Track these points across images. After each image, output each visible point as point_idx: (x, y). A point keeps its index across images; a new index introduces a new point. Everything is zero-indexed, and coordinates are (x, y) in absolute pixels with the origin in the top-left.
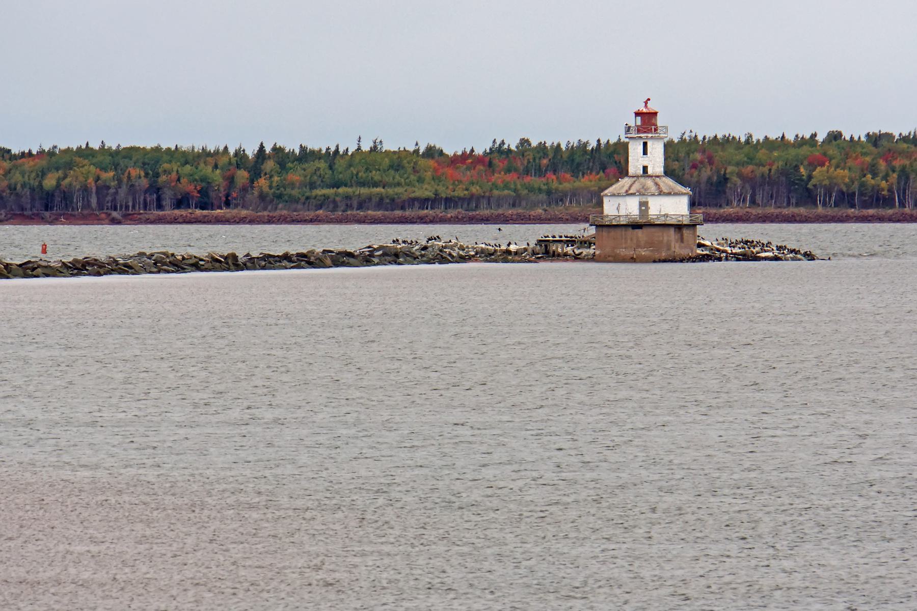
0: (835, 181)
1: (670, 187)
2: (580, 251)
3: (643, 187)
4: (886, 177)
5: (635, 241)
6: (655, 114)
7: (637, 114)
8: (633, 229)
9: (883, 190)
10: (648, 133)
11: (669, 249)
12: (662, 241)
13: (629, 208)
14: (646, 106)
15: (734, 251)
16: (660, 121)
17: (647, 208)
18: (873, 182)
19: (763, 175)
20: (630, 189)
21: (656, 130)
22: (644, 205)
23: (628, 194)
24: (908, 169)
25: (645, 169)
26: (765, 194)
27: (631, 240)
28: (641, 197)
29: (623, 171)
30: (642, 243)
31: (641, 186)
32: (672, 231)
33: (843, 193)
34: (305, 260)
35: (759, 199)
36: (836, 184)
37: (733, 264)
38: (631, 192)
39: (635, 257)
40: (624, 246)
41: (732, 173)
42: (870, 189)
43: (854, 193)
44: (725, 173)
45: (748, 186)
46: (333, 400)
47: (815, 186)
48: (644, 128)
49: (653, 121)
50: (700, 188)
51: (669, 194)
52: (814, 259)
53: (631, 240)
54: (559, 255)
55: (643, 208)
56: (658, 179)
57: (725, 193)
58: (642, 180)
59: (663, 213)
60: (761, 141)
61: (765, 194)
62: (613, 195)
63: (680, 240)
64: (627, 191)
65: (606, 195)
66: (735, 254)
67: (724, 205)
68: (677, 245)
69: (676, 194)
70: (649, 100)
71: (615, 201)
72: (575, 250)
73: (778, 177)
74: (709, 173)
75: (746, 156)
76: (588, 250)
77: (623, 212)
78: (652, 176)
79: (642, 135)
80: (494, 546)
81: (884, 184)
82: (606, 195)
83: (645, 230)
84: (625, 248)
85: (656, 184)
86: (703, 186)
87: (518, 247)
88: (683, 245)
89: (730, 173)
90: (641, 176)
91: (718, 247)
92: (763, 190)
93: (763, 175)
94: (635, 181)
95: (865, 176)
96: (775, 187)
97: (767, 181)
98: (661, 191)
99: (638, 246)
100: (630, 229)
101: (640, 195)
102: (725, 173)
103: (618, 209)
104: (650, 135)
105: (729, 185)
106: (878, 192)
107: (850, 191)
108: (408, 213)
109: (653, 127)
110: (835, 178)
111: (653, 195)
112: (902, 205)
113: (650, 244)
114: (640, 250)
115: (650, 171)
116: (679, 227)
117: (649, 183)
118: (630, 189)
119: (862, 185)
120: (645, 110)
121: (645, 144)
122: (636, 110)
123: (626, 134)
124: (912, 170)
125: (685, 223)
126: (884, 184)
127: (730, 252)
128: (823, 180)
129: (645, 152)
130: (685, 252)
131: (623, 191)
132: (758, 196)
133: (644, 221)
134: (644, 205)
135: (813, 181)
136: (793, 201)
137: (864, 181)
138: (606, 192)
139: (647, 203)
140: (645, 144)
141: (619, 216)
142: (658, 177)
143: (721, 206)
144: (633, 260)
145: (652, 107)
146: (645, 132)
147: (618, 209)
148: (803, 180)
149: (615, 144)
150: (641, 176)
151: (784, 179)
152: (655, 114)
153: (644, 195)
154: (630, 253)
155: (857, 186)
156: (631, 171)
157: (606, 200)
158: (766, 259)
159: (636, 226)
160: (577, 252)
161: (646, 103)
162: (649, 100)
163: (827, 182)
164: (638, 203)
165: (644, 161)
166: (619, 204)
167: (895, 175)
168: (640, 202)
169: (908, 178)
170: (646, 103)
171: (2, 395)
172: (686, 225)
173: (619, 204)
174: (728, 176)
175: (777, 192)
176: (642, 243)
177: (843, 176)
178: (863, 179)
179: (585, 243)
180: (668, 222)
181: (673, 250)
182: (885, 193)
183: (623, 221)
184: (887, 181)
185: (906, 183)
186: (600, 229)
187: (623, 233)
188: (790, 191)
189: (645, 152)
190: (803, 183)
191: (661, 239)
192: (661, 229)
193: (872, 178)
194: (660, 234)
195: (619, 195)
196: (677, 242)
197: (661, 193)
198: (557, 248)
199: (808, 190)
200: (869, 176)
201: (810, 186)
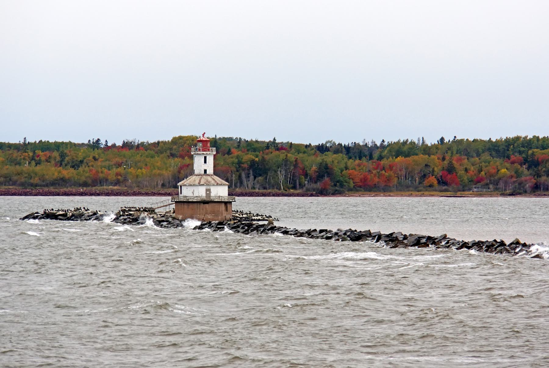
1: (221, 182)
3: (207, 181)
8: (203, 204)
13: (200, 193)
17: (210, 192)
20: (200, 181)
22: (208, 191)
23: (200, 184)
25: (205, 171)
27: (203, 209)
29: (192, 173)
31: (206, 181)
34: (50, 215)
38: (201, 183)
46: (102, 300)
51: (221, 185)
55: (208, 192)
58: (204, 177)
60: (528, 138)
70: (205, 133)
71: (191, 189)
77: (196, 194)
78: (209, 175)
79: (204, 153)
80: (256, 313)
87: (259, 191)
94: (201, 178)
99: (206, 213)
100: (202, 204)
103: (193, 193)
104: (208, 153)
108: (94, 189)
111: (214, 185)
118: (200, 181)
121: (205, 158)
129: (205, 162)
134: (208, 191)
140: (205, 158)
147: (193, 193)
149: (530, 140)
156: (196, 172)
159: (205, 202)
162: (205, 133)
165: (205, 167)
170: (203, 135)
176: (209, 211)
186: (179, 205)
189: (205, 162)
194: (218, 207)
195: (194, 185)
197: (218, 184)
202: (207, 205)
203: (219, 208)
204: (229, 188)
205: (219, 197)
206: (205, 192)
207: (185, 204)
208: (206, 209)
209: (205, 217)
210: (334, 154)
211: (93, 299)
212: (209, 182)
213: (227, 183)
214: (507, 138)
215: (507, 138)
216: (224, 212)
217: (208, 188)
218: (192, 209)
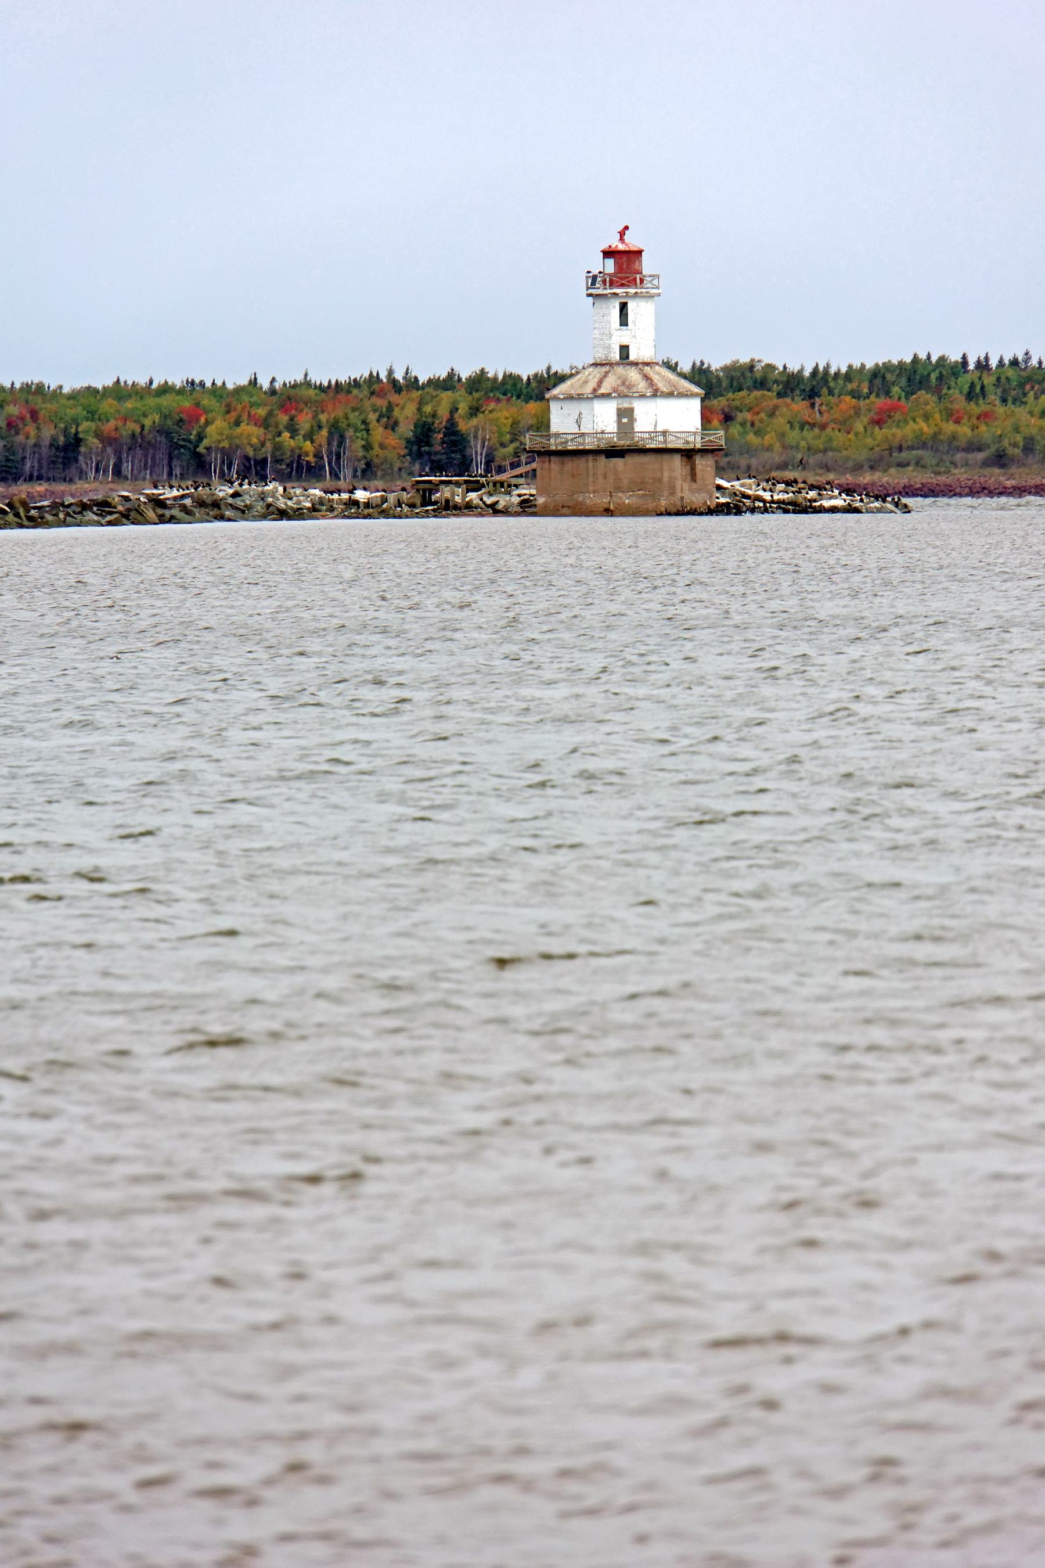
0: (237, 441)
1: (669, 382)
2: (493, 499)
3: (623, 383)
4: (309, 436)
5: (611, 478)
6: (639, 253)
7: (608, 254)
9: (307, 455)
10: (629, 286)
11: (673, 493)
12: (660, 480)
14: (622, 239)
15: (776, 497)
16: (648, 265)
17: (632, 420)
18: (292, 443)
19: (133, 435)
20: (600, 383)
21: (642, 281)
22: (625, 415)
23: (597, 395)
24: (343, 425)
25: (624, 349)
26: (136, 461)
27: (605, 476)
28: (620, 401)
30: (625, 482)
31: (619, 382)
32: (677, 459)
33: (247, 458)
35: (127, 468)
36: (238, 447)
37: (780, 518)
38: (602, 391)
39: (612, 507)
40: (591, 488)
41: (86, 432)
42: (289, 454)
43: (265, 460)
44: (77, 433)
45: (109, 450)
47: (208, 449)
48: (621, 278)
49: (636, 266)
50: (40, 454)
51: (670, 395)
52: (909, 512)
53: (605, 476)
54: (456, 507)
55: (625, 420)
56: (647, 369)
57: (76, 461)
58: (620, 370)
59: (660, 429)
61: (136, 461)
62: (570, 398)
63: (689, 478)
64: (595, 390)
65: (556, 398)
66: (778, 502)
67: (77, 480)
68: (686, 486)
69: (682, 395)
70: (626, 228)
72: (485, 499)
73: (155, 437)
74: (53, 432)
75: (84, 409)
76: (508, 498)
78: (636, 364)
81: (308, 446)
82: (556, 398)
83: (631, 460)
84: (594, 492)
85: (646, 377)
86: (45, 450)
88: (695, 486)
89: (83, 432)
90: (618, 364)
91: (743, 489)
92: (134, 457)
93: (133, 435)
94: (607, 373)
95: (279, 435)
96: (151, 451)
97: (138, 443)
98: (657, 390)
99: (619, 489)
100: (602, 459)
101: (619, 396)
102: (77, 433)
103: (578, 423)
104: (632, 291)
105: (82, 449)
106: (299, 456)
107: (259, 457)
109: (638, 276)
110: (237, 437)
111: (643, 396)
112: (336, 476)
113: (638, 485)
114: (620, 494)
115: (632, 357)
116: (688, 454)
117: (633, 375)
118: (600, 383)
119: (278, 447)
120: (621, 247)
121: (623, 307)
122: (605, 246)
123: (588, 289)
124: (349, 425)
125: (698, 446)
126: (308, 446)
127: (769, 498)
128: (220, 442)
129: (624, 321)
130: (697, 499)
131: (588, 390)
132: (125, 465)
133: (628, 443)
134: (625, 415)
135: (205, 443)
136: (177, 471)
137: (279, 442)
138: (555, 392)
139: (632, 410)
140: (623, 307)
141: (583, 434)
142: (647, 364)
143: (71, 481)
144: (608, 512)
145: (633, 241)
146: (622, 285)
147: (578, 423)
148: (190, 441)
150: (618, 364)
151: (163, 439)
152: (639, 253)
153: (626, 396)
154: (604, 501)
155: (270, 450)
157: (554, 407)
158: (833, 510)
159: (613, 452)
160: (489, 501)
161: (622, 234)
162: (626, 228)
163: (225, 444)
164: (615, 412)
166: (580, 414)
167: (324, 432)
168: (619, 410)
169: (342, 437)
170: (622, 234)
171: (5, 771)
172: (700, 451)
173: (580, 414)
174: (81, 436)
175: (153, 459)
176: (625, 482)
177: (251, 433)
178: (277, 439)
179: (502, 486)
180: (670, 446)
181: (680, 495)
182: (311, 458)
183: (590, 444)
184: (312, 442)
185: (339, 446)
187: (591, 464)
188: (170, 459)
189: (624, 321)
190: (191, 446)
191: (659, 475)
192: (659, 457)
193: (292, 437)
194: (657, 466)
195: (580, 398)
196: (685, 481)
197: (656, 394)
198: (453, 494)
199: (197, 456)
200: (286, 435)
201: (201, 449)
202: (618, 462)
203: (662, 470)
204: (703, 400)
205: (664, 433)
206: (614, 418)
207: (553, 458)
208: (616, 473)
209: (614, 499)
210: (627, 325)
211: (564, 794)
212: (629, 387)
213: (696, 389)
214: (166, 382)
215: (166, 382)
216: (679, 483)
217: (626, 405)
218: (573, 476)
